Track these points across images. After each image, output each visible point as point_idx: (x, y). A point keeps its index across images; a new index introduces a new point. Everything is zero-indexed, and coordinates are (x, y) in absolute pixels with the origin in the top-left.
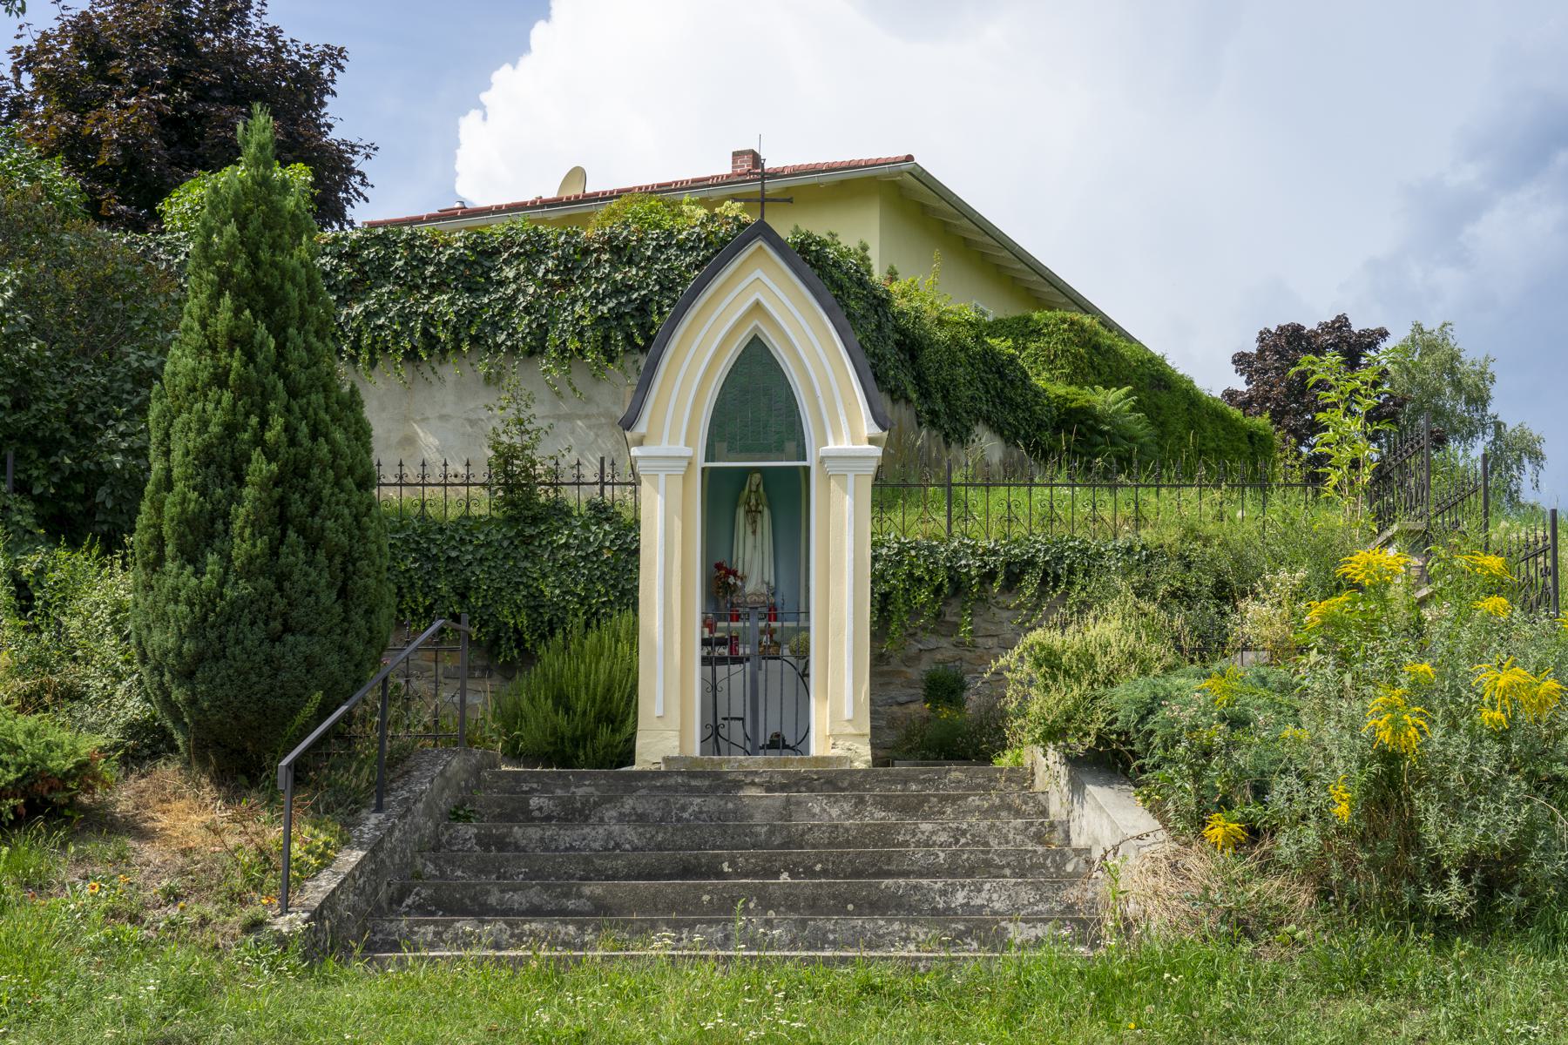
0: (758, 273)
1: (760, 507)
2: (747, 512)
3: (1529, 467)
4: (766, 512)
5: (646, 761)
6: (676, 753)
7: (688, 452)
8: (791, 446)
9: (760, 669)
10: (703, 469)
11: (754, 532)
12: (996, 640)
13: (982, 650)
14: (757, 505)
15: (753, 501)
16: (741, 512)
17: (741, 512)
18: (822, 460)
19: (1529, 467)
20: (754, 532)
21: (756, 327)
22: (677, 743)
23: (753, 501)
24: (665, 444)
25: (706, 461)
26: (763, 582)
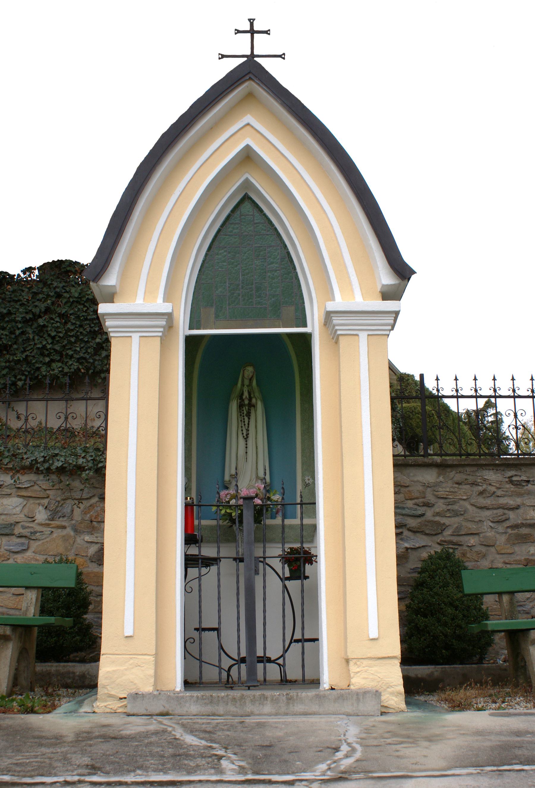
0: (248, 118)
1: (254, 400)
2: (241, 406)
3: (11, 751)
4: (260, 406)
5: (111, 696)
6: (148, 688)
7: (166, 308)
8: (289, 311)
9: (257, 572)
10: (190, 340)
11: (246, 439)
12: (476, 538)
13: (465, 548)
14: (250, 399)
15: (246, 394)
16: (234, 406)
17: (234, 406)
18: (329, 315)
19: (11, 751)
20: (246, 439)
21: (247, 181)
22: (152, 672)
23: (246, 394)
24: (139, 300)
25: (191, 328)
26: (257, 478)
